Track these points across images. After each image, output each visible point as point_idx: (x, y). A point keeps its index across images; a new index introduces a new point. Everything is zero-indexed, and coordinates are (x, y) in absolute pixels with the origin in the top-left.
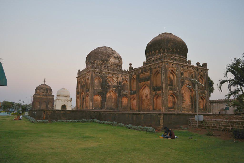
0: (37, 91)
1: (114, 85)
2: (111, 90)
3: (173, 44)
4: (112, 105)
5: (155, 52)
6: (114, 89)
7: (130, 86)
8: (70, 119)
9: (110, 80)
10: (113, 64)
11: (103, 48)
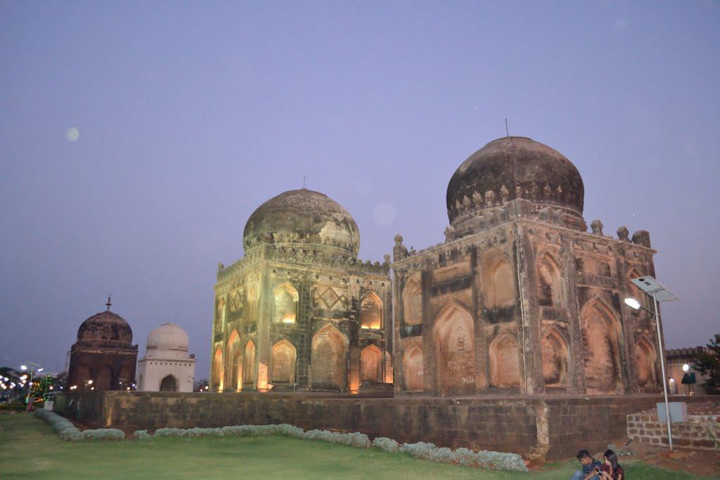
0: (86, 332)
1: (334, 311)
2: (328, 325)
3: (541, 169)
5: (483, 195)
6: (335, 323)
7: (399, 308)
8: (200, 426)
9: (323, 294)
10: (330, 245)
11: (298, 195)
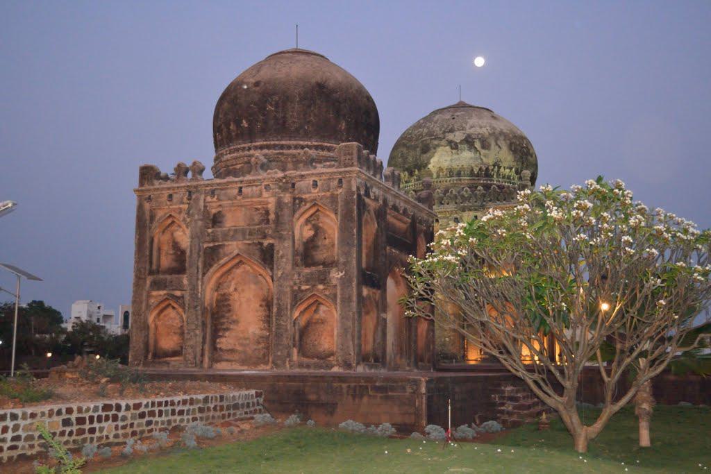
4: (445, 341)
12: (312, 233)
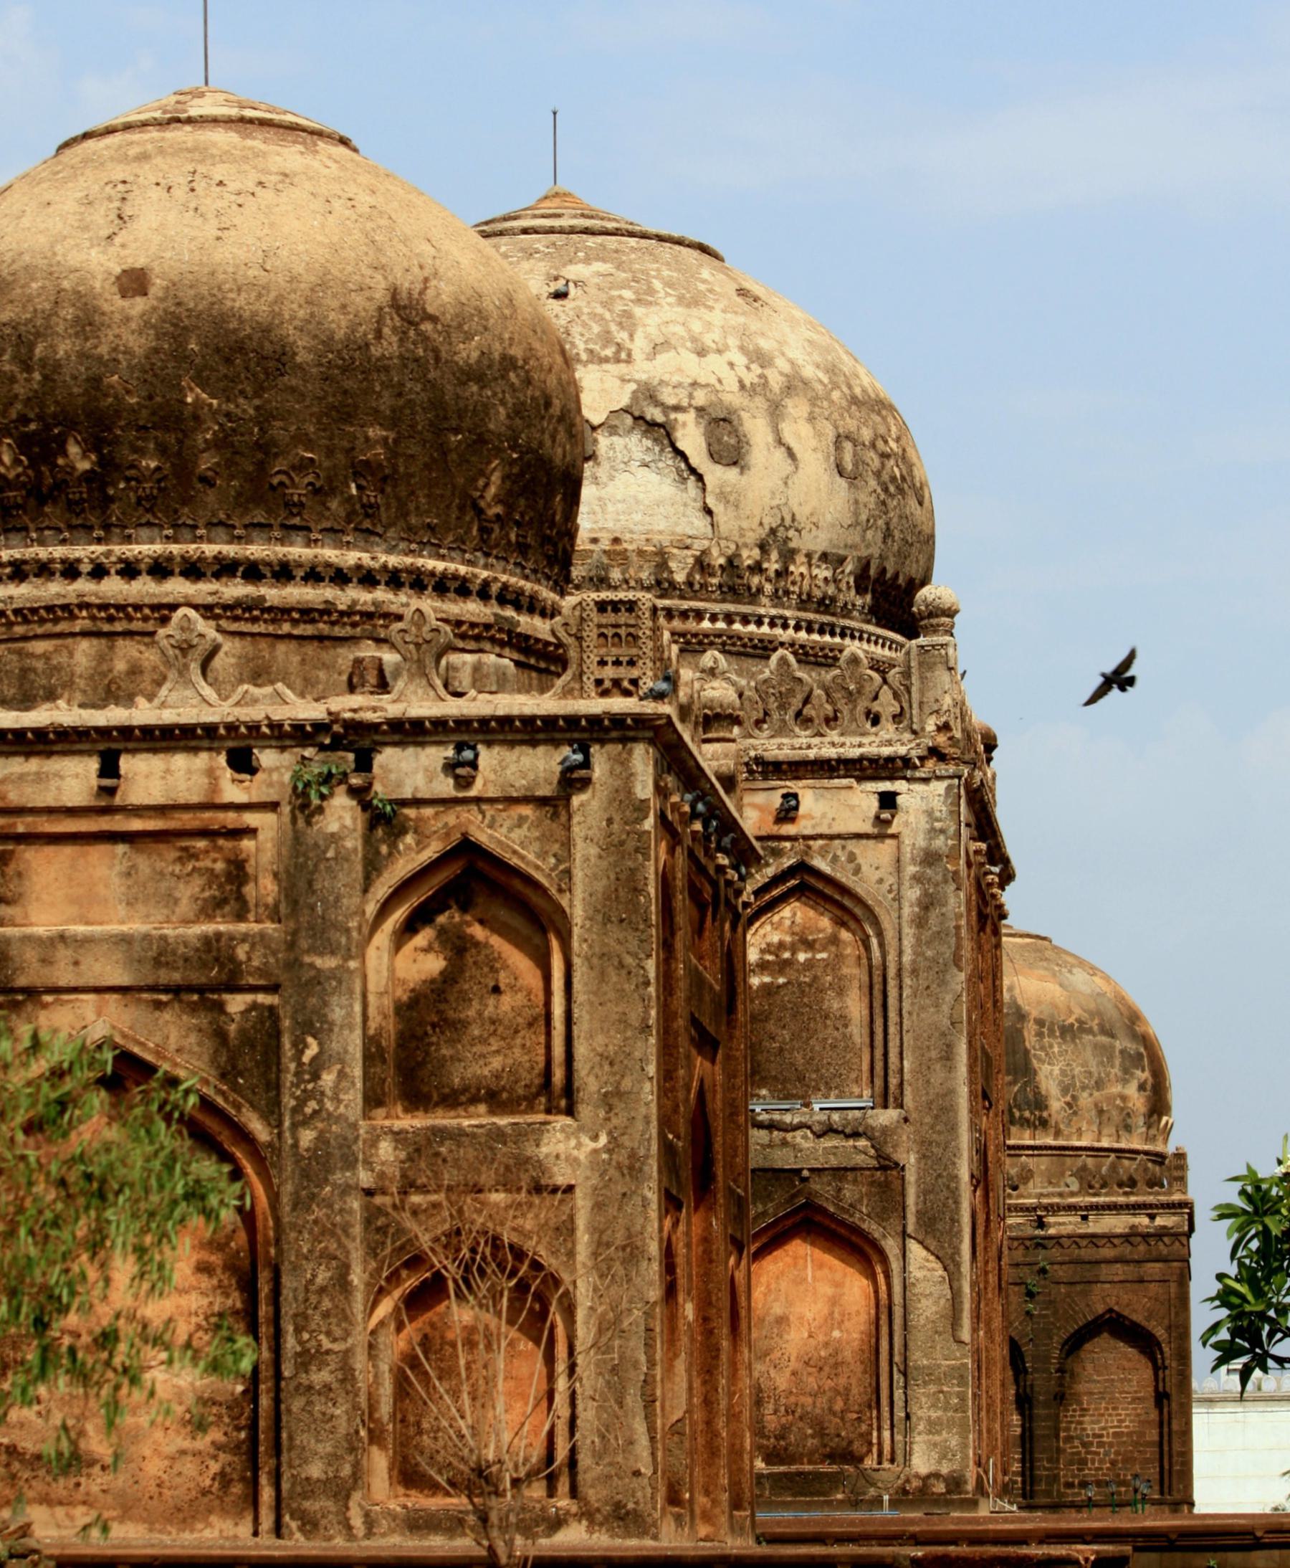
12: (434, 964)
